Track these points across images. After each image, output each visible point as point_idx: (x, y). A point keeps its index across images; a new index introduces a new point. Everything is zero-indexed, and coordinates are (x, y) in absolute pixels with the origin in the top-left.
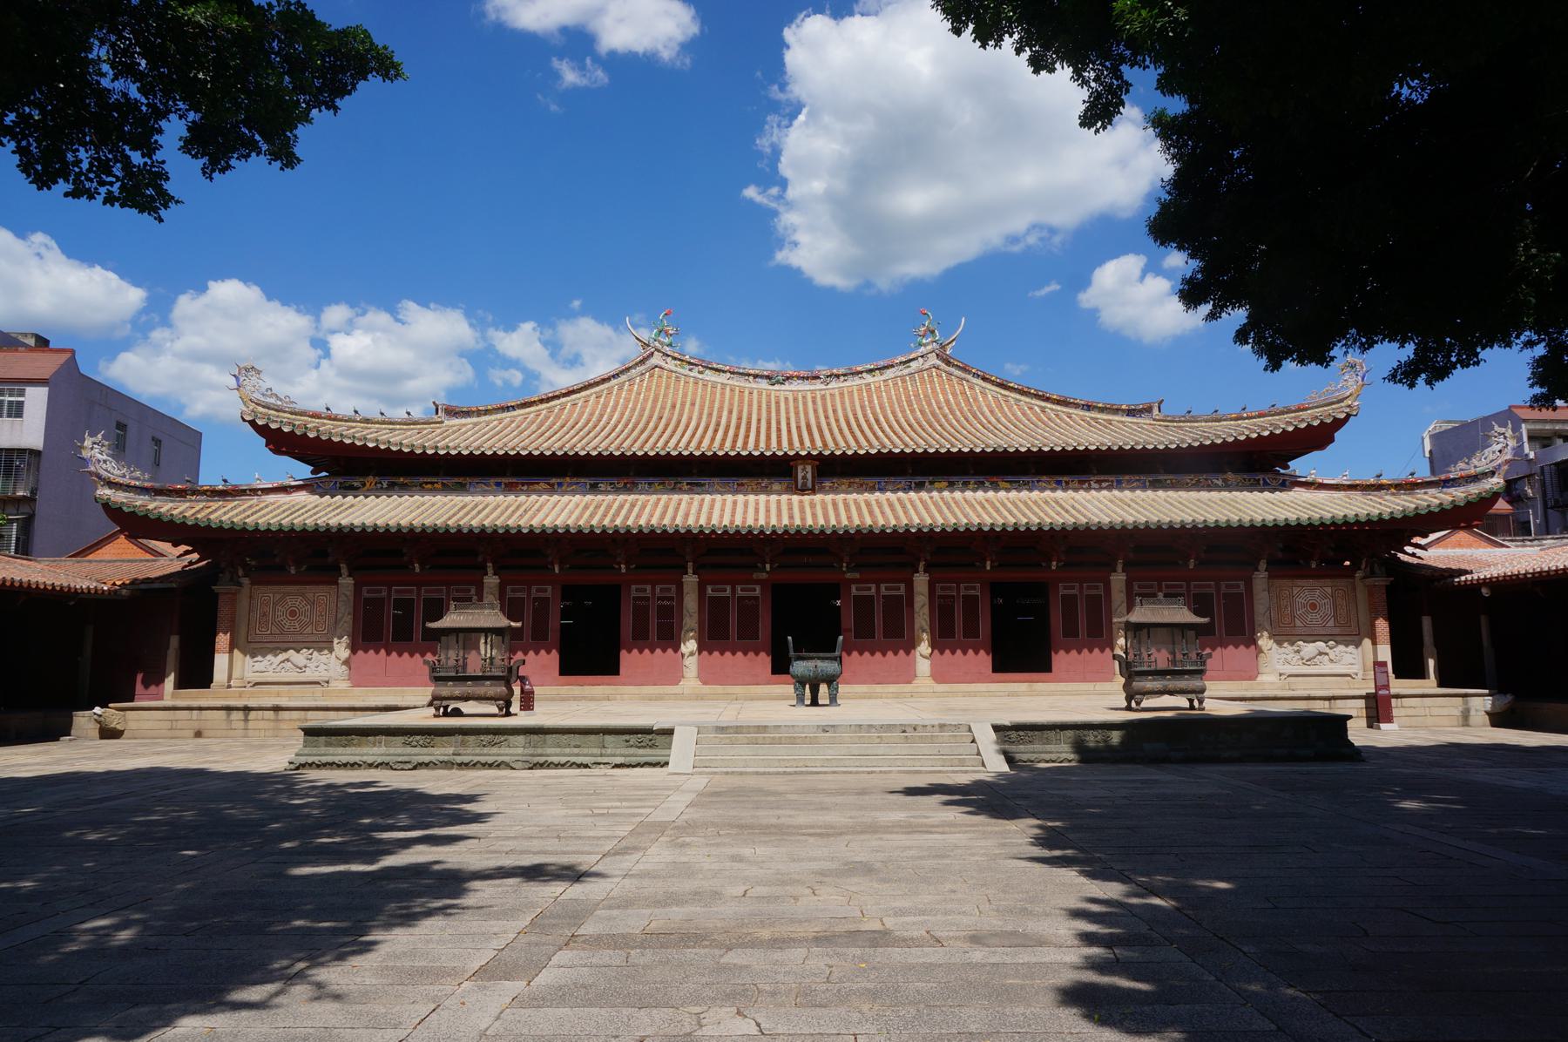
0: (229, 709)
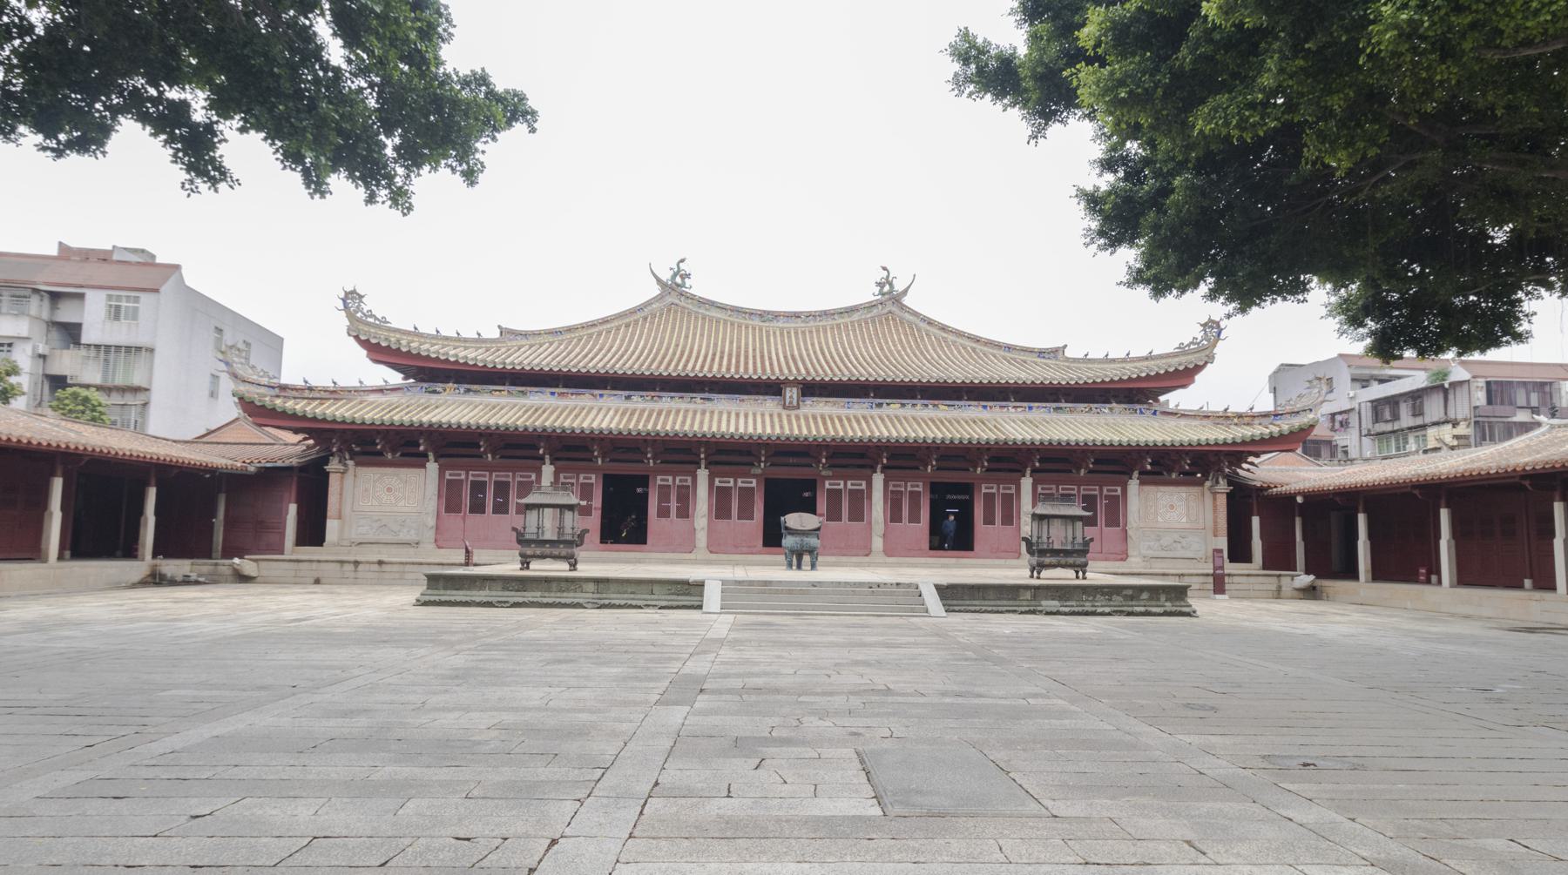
0: (342, 562)
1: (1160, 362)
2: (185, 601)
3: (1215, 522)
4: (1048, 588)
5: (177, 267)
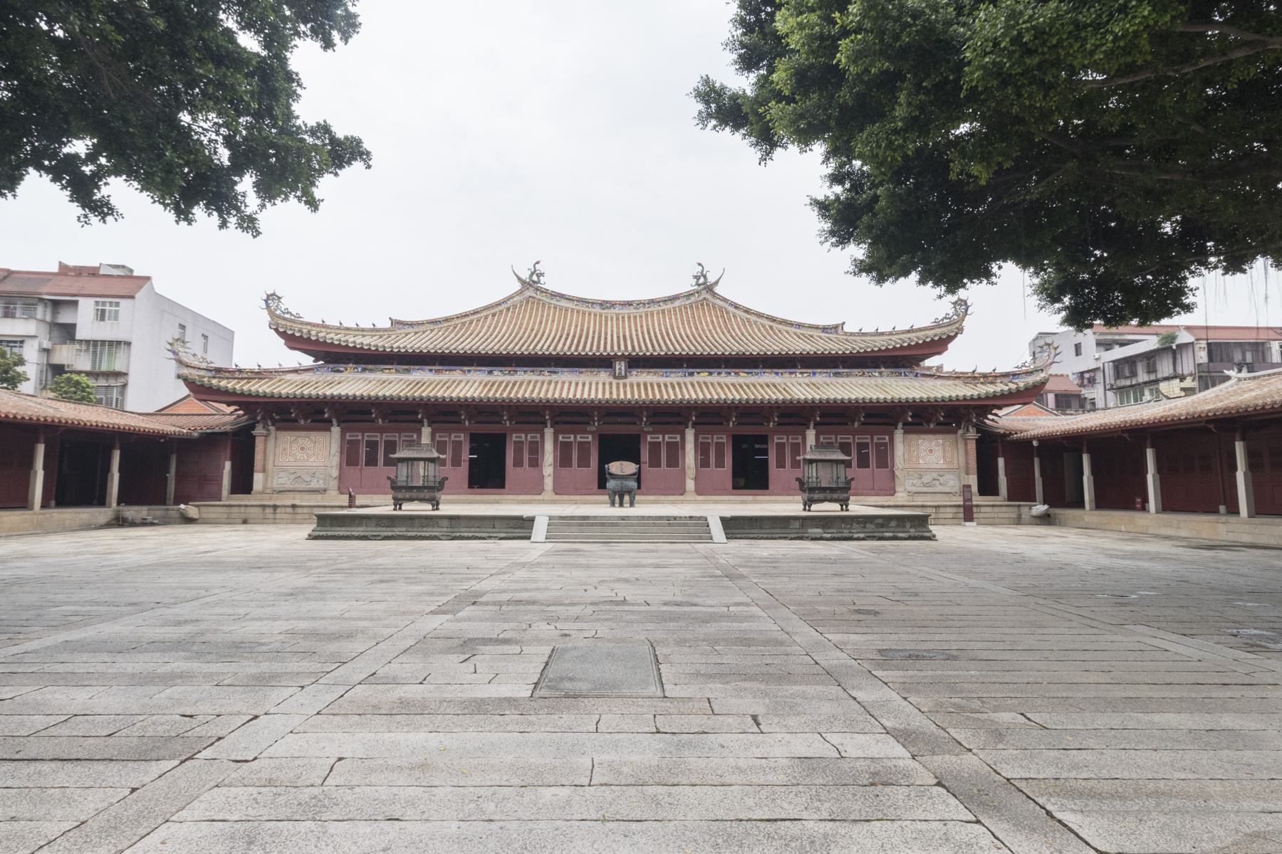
0: (264, 506)
1: (920, 334)
2: (131, 538)
3: (967, 463)
4: (813, 518)
5: (148, 279)
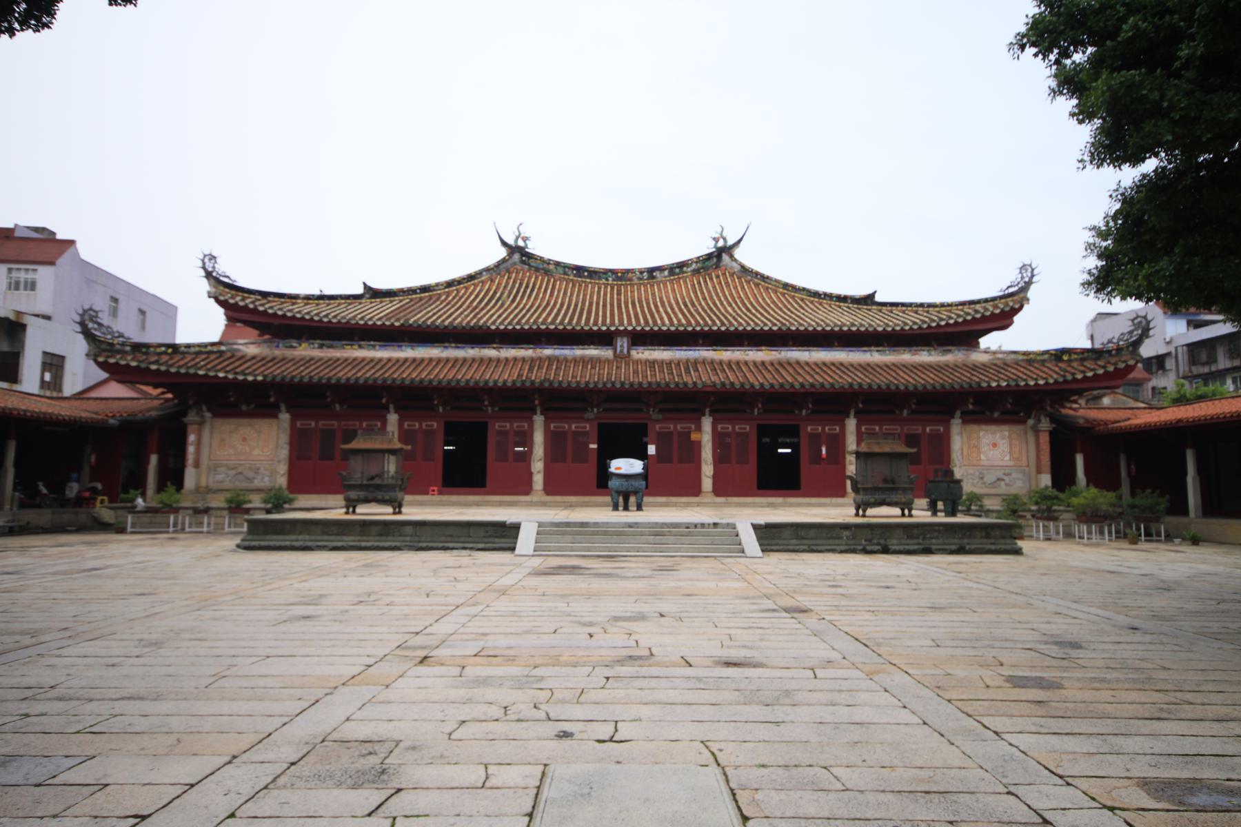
5: (71, 243)
